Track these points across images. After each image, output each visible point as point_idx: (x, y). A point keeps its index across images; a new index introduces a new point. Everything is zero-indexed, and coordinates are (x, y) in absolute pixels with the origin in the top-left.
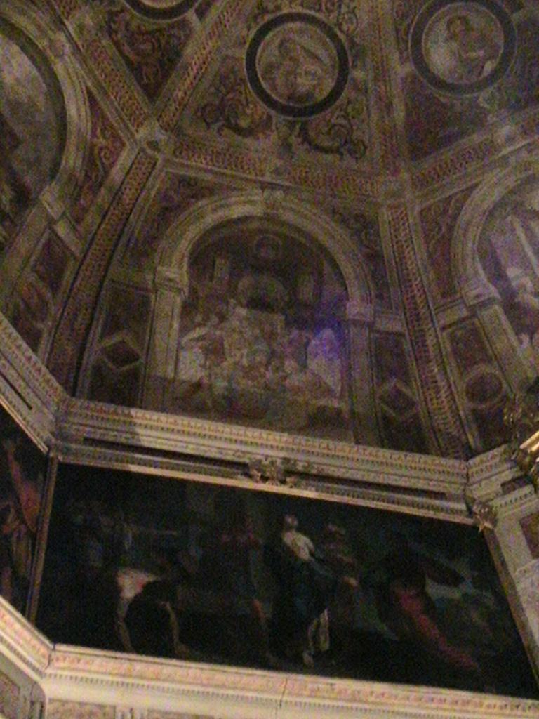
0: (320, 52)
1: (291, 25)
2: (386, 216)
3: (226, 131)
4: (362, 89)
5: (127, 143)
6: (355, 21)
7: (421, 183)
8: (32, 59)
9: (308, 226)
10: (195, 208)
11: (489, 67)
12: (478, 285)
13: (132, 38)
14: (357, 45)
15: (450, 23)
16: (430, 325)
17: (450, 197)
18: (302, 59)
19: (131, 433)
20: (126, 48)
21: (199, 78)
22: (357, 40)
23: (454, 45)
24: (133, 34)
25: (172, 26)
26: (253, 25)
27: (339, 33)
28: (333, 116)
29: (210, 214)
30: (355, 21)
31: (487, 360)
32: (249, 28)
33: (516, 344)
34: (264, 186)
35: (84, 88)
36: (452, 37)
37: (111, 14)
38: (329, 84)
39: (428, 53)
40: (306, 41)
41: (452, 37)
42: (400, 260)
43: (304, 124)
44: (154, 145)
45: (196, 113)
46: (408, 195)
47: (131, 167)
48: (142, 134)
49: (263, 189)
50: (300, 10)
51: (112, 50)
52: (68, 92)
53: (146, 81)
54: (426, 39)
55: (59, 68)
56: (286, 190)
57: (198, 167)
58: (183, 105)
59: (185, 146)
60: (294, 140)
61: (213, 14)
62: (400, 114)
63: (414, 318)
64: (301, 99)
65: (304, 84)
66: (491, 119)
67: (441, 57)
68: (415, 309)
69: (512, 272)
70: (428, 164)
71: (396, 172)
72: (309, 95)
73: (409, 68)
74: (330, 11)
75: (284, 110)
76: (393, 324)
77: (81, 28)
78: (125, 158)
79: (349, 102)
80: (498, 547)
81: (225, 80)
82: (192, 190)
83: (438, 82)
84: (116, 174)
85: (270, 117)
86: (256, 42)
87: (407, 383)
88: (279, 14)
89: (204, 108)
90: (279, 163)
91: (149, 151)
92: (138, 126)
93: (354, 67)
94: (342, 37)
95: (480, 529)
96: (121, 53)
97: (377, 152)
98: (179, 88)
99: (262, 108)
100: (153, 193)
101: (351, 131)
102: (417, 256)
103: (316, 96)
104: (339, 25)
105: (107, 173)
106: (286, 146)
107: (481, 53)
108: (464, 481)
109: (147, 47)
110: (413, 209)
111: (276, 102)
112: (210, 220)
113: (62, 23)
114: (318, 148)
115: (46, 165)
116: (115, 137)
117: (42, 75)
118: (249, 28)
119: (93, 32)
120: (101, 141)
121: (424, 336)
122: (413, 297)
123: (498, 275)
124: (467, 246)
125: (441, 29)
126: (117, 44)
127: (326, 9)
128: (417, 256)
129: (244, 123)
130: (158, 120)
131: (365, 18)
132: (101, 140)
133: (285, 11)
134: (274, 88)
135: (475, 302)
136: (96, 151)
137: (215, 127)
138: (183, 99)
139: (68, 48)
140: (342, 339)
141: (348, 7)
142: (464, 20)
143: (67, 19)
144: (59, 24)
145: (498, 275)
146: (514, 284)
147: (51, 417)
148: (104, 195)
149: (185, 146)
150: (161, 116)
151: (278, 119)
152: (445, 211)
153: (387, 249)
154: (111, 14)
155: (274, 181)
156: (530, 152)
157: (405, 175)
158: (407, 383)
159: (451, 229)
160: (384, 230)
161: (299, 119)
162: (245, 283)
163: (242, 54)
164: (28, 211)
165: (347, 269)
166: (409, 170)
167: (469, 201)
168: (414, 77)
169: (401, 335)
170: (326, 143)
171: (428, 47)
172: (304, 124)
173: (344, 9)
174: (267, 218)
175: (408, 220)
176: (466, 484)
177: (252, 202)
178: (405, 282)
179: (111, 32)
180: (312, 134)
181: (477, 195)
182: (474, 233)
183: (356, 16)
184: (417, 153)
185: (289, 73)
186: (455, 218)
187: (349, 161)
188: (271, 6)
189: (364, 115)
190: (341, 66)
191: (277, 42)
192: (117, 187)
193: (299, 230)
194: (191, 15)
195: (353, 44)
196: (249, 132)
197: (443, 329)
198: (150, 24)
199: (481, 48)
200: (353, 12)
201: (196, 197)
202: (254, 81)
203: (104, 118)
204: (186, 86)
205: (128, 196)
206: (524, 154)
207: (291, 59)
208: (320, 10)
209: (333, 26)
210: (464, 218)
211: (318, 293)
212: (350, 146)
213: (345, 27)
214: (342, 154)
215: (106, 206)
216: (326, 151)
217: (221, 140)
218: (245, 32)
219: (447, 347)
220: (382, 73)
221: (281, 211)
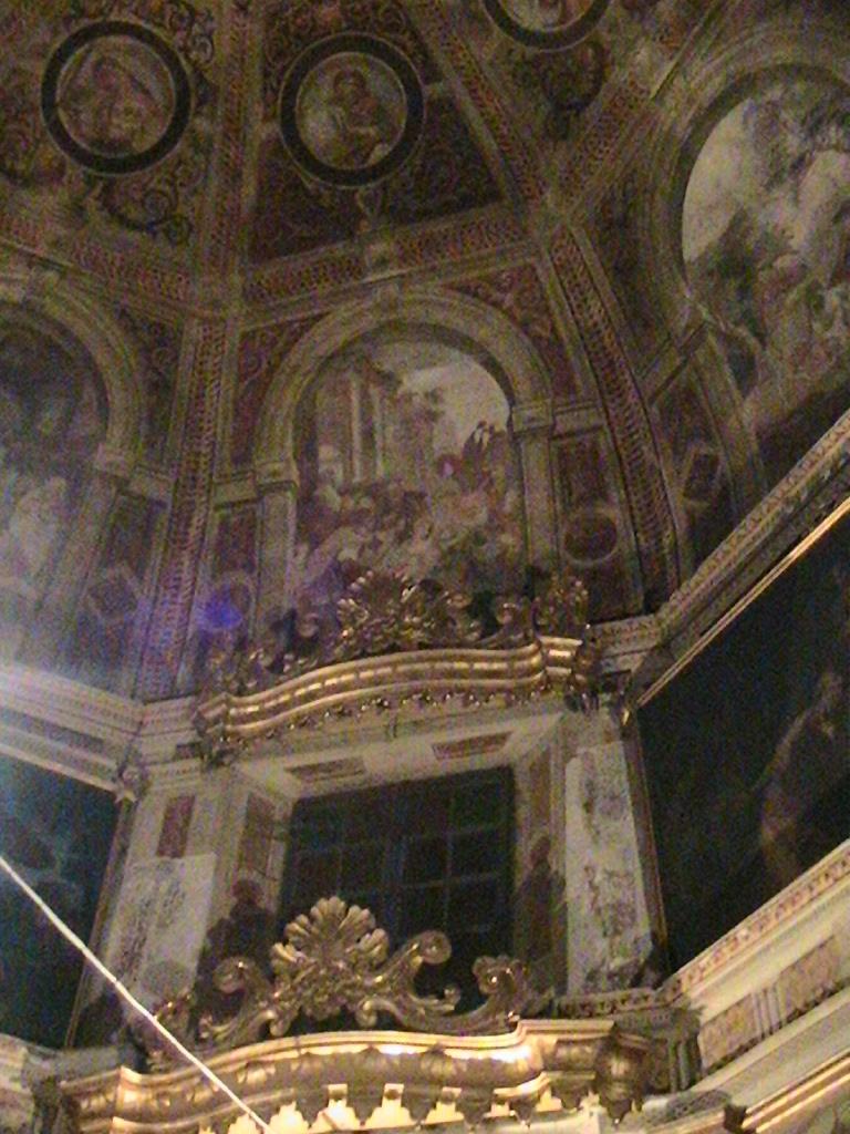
0: (151, 83)
1: (114, 40)
2: (195, 331)
4: (202, 146)
6: (209, 50)
7: (253, 295)
9: (80, 329)
11: (379, 153)
12: (278, 461)
15: (337, 80)
16: (204, 499)
18: (122, 90)
22: (207, 76)
23: (339, 111)
26: (62, 28)
27: (183, 62)
28: (153, 177)
30: (209, 50)
31: (250, 567)
32: (55, 32)
33: (290, 552)
34: (31, 261)
36: (337, 100)
39: (302, 116)
40: (131, 64)
41: (337, 100)
42: (197, 397)
43: (112, 182)
49: (30, 265)
50: (133, 20)
54: (304, 93)
56: (63, 274)
60: (92, 203)
62: (249, 190)
63: (188, 483)
64: (113, 145)
65: (120, 127)
66: (365, 227)
67: (319, 126)
68: (195, 471)
69: (326, 452)
70: (268, 272)
72: (124, 144)
73: (273, 129)
74: (175, 29)
75: (83, 158)
76: (153, 487)
79: (180, 163)
80: (126, 833)
83: (304, 155)
85: (62, 165)
86: (60, 57)
87: (139, 572)
90: (62, 232)
93: (198, 113)
94: (188, 70)
95: (118, 800)
99: (52, 151)
101: (173, 207)
103: (134, 145)
104: (186, 50)
106: (77, 210)
107: (372, 131)
108: (134, 730)
111: (389, 62)
114: (124, 221)
118: (55, 32)
121: (193, 510)
123: (307, 451)
124: (284, 401)
127: (171, 24)
131: (224, 49)
134: (77, 124)
135: (268, 481)
140: (75, 495)
141: (204, 28)
142: (361, 82)
145: (307, 451)
146: (322, 469)
151: (75, 170)
152: (274, 342)
153: (184, 384)
155: (52, 257)
156: (402, 286)
158: (139, 572)
159: (271, 371)
160: (187, 352)
161: (103, 174)
163: (40, 69)
165: (117, 399)
166: (242, 272)
167: (306, 335)
169: (161, 504)
170: (134, 214)
171: (306, 104)
173: (196, 28)
174: (25, 306)
176: (135, 734)
178: (193, 429)
180: (118, 200)
181: (318, 330)
183: (212, 42)
184: (261, 252)
186: (282, 355)
187: (161, 247)
188: (92, 9)
193: (64, 331)
196: (28, 181)
197: (217, 508)
199: (373, 124)
200: (209, 36)
202: (49, 105)
206: (393, 289)
207: (108, 88)
208: (160, 25)
209: (176, 50)
210: (294, 357)
212: (167, 224)
213: (193, 55)
214: (155, 234)
216: (136, 227)
219: (213, 533)
220: (235, 129)
221: (48, 299)
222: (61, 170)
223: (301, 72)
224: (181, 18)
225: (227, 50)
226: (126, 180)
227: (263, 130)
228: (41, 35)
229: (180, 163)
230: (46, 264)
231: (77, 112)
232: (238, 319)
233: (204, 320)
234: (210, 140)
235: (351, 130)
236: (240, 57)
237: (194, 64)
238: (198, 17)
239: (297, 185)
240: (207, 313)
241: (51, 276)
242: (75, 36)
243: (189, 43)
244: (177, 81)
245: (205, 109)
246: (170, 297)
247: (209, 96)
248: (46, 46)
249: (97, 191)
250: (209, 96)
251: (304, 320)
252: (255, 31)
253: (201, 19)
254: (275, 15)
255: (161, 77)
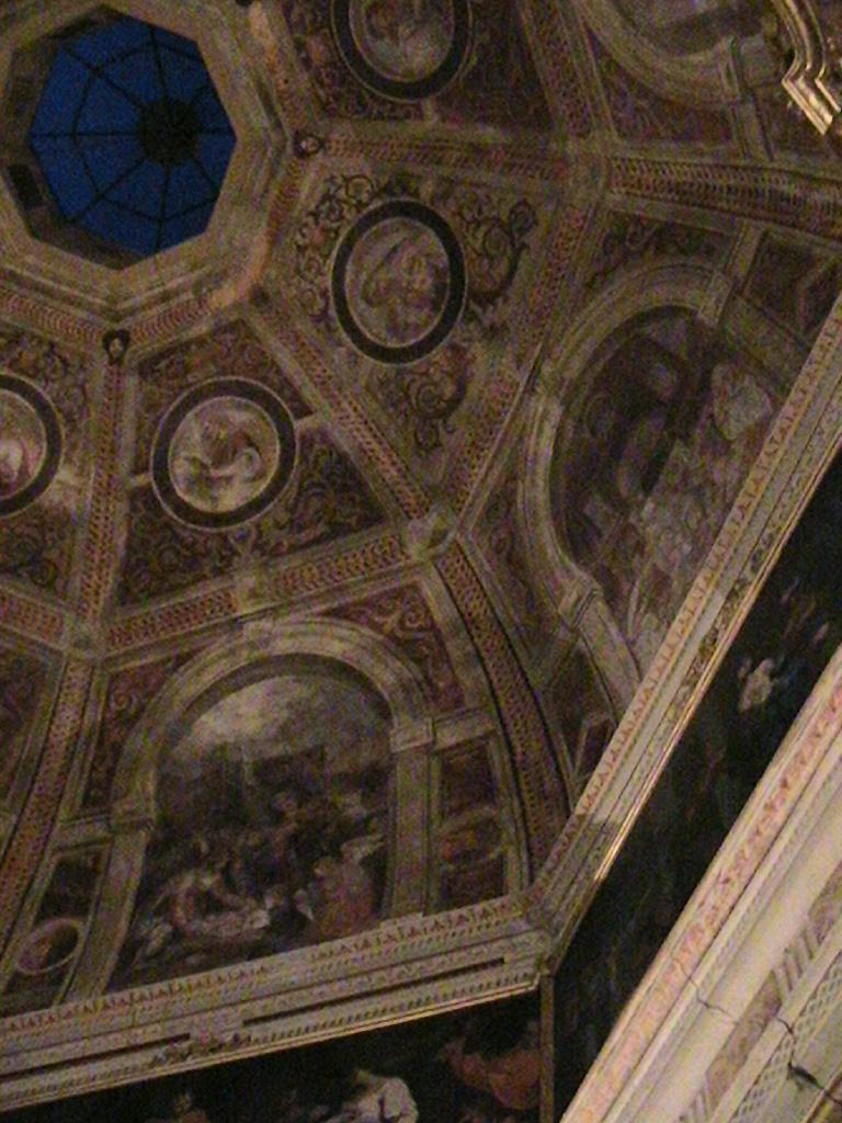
2: (615, 197)
3: (453, 420)
4: (448, 186)
5: (416, 578)
8: (252, 681)
9: (602, 330)
10: (521, 514)
13: (295, 525)
14: (390, 182)
16: (766, 176)
17: (604, 80)
19: (601, 831)
20: (303, 537)
21: (379, 434)
22: (384, 180)
23: (403, 30)
24: (291, 521)
25: (304, 459)
27: (371, 207)
28: (473, 242)
29: (536, 491)
32: (340, 343)
34: (530, 390)
35: (319, 619)
37: (256, 546)
38: (432, 240)
40: (370, 262)
43: (474, 296)
44: (437, 538)
45: (420, 456)
46: (597, 148)
47: (448, 588)
48: (415, 550)
50: (331, 263)
51: (296, 561)
52: (309, 645)
53: (353, 521)
55: (283, 646)
57: (481, 479)
58: (405, 473)
59: (449, 491)
61: (310, 393)
62: (490, 134)
64: (439, 289)
65: (423, 281)
70: (560, 105)
71: (564, 160)
72: (438, 273)
73: (428, 105)
74: (341, 218)
75: (447, 323)
77: (254, 594)
78: (432, 589)
81: (396, 398)
82: (502, 503)
83: (448, 67)
84: (442, 612)
88: (330, 294)
89: (419, 444)
91: (441, 548)
92: (403, 553)
93: (416, 194)
96: (307, 545)
97: (536, 185)
98: (386, 470)
99: (438, 354)
100: (487, 568)
102: (680, 162)
104: (360, 205)
105: (433, 626)
106: (494, 333)
109: (315, 503)
110: (615, 145)
111: (435, 331)
112: (541, 496)
113: (236, 620)
115: (369, 718)
116: (398, 594)
117: (264, 677)
118: (340, 343)
119: (265, 578)
120: (391, 622)
122: (729, 188)
125: (382, 47)
126: (293, 549)
127: (337, 220)
128: (680, 162)
129: (449, 390)
130: (410, 518)
132: (390, 620)
133: (329, 282)
134: (418, 328)
136: (399, 634)
137: (444, 438)
138: (399, 470)
139: (266, 624)
143: (235, 611)
144: (236, 624)
147: (534, 935)
148: (456, 648)
149: (449, 491)
150: (407, 512)
151: (456, 335)
153: (659, 211)
154: (256, 546)
157: (571, 147)
160: (639, 206)
162: (624, 483)
164: (391, 785)
168: (438, 99)
170: (503, 268)
172: (474, 296)
173: (342, 194)
175: (630, 160)
177: (544, 417)
179: (276, 553)
181: (604, 36)
182: (648, 51)
184: (542, 119)
185: (405, 303)
186: (630, 80)
189: (481, 192)
190: (407, 214)
191: (363, 305)
192: (458, 615)
193: (596, 356)
194: (300, 425)
195: (387, 189)
198: (290, 490)
200: (347, 180)
201: (511, 503)
203: (367, 603)
204: (385, 459)
205: (476, 607)
210: (629, 64)
211: (672, 359)
212: (515, 228)
213: (364, 197)
215: (470, 648)
217: (460, 429)
218: (343, 350)
220: (431, 151)
222: (453, 347)
223: (371, 76)
224: (332, 210)
225: (361, 159)
226: (472, 271)
227: (430, 120)
228: (339, 355)
229: (460, 214)
230: (535, 372)
231: (407, 325)
232: (606, 142)
233: (608, 185)
234: (443, 179)
235: (417, 16)
236: (363, 146)
237: (374, 196)
238: (332, 192)
239: (476, 75)
240: (601, 182)
241: (547, 369)
242: (343, 323)
243: (354, 202)
244: (386, 216)
245: (413, 184)
246: (582, 228)
247: (402, 182)
248: (351, 354)
249: (479, 310)
250: (402, 182)
251: (596, 55)
252: (342, 132)
253: (333, 189)
254: (324, 109)
255: (385, 232)
